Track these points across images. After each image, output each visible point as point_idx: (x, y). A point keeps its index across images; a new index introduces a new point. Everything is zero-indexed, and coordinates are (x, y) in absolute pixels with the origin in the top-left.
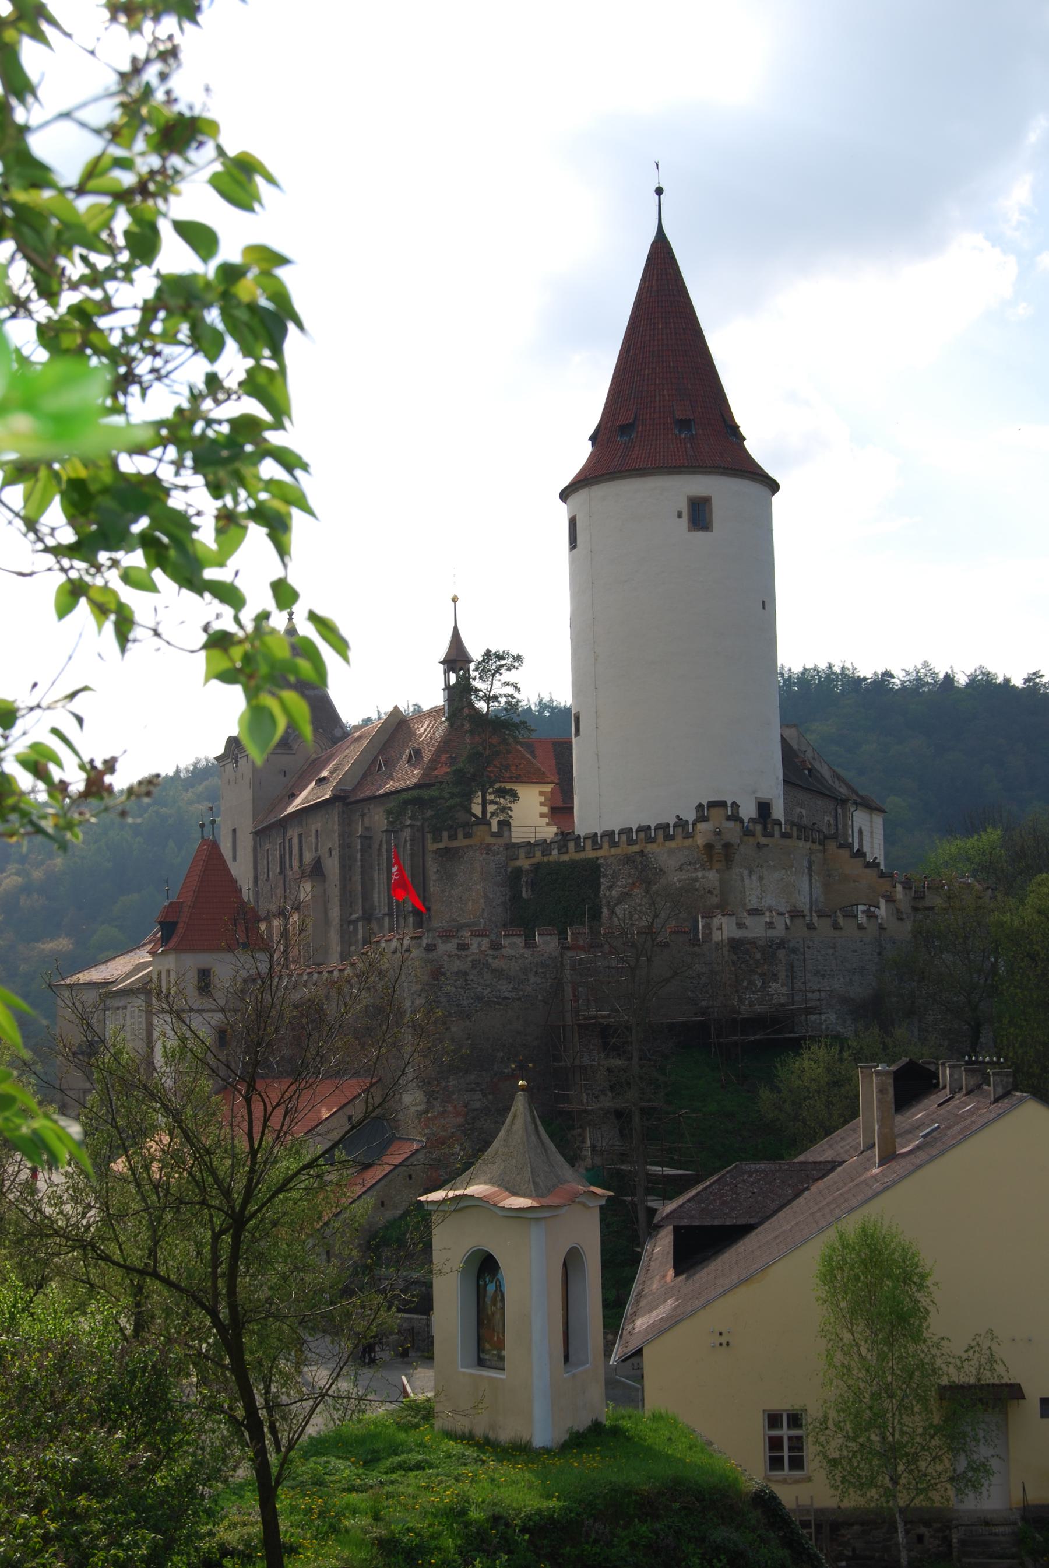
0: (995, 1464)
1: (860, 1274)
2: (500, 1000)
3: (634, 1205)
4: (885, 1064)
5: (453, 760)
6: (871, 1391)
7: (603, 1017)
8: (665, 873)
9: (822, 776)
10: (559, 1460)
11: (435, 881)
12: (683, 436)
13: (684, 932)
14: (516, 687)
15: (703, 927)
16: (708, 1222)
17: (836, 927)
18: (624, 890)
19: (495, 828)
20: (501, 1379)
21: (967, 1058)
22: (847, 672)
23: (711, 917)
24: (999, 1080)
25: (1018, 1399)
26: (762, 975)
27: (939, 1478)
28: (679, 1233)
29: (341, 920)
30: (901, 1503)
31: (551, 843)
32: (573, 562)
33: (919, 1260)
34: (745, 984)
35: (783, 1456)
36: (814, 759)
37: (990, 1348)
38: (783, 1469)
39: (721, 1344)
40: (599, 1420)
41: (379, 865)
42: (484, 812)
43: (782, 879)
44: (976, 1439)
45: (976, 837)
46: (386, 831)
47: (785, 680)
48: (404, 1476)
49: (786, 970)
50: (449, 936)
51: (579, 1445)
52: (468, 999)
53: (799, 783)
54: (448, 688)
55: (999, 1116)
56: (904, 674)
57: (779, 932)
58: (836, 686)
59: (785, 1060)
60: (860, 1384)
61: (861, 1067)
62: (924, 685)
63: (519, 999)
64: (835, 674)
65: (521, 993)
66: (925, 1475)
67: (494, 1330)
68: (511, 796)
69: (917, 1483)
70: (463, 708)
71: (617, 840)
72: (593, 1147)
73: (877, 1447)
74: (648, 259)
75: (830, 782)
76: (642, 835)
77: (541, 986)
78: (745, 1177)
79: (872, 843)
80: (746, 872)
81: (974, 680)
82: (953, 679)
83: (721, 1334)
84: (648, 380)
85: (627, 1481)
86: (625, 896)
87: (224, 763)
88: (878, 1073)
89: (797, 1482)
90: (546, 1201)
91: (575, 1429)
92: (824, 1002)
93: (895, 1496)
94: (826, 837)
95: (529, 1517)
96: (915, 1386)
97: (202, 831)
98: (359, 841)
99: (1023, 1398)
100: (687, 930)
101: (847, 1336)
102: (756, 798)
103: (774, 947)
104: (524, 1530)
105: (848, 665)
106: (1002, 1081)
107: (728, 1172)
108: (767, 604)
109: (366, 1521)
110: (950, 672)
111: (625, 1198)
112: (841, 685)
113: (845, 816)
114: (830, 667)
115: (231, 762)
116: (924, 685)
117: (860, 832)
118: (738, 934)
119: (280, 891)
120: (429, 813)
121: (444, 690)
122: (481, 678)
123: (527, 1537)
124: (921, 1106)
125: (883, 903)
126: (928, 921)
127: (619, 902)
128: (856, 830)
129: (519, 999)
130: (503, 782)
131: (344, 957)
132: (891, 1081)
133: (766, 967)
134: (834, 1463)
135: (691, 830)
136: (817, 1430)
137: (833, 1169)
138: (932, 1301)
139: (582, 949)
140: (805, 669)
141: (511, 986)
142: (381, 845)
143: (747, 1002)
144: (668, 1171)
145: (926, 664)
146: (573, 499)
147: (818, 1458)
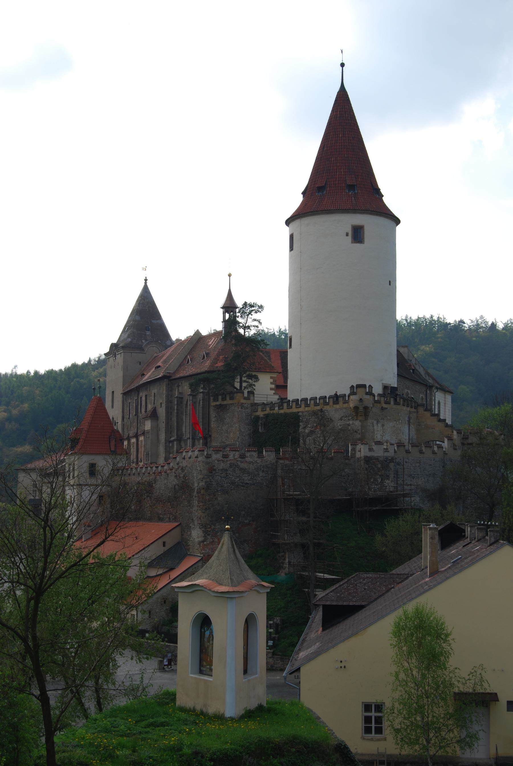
0: (481, 734)
1: (414, 632)
2: (244, 485)
4: (434, 524)
6: (417, 694)
7: (296, 495)
8: (333, 421)
9: (420, 373)
10: (237, 724)
11: (214, 422)
12: (350, 193)
13: (341, 452)
14: (259, 322)
15: (351, 450)
16: (340, 603)
17: (421, 452)
19: (246, 395)
20: (210, 681)
21: (479, 522)
22: (440, 320)
23: (356, 445)
24: (492, 534)
25: (496, 701)
26: (381, 476)
27: (452, 741)
28: (326, 608)
29: (166, 440)
30: (432, 753)
31: (275, 404)
32: (291, 257)
33: (444, 627)
34: (372, 480)
35: (371, 727)
36: (416, 364)
37: (480, 674)
38: (371, 733)
39: (341, 667)
40: (262, 704)
41: (186, 412)
42: (241, 386)
43: (394, 426)
44: (471, 721)
45: (498, 408)
46: (190, 395)
47: (408, 323)
48: (153, 729)
51: (250, 717)
53: (407, 376)
54: (224, 321)
55: (491, 553)
56: (470, 321)
58: (434, 327)
59: (390, 520)
60: (412, 690)
61: (424, 525)
62: (480, 328)
63: (254, 484)
64: (434, 320)
66: (444, 739)
68: (255, 378)
69: (440, 743)
70: (231, 332)
71: (309, 403)
72: (289, 562)
73: (420, 723)
74: (336, 100)
75: (424, 376)
76: (322, 401)
77: (266, 478)
79: (445, 409)
80: (375, 422)
81: (506, 326)
82: (496, 325)
83: (341, 662)
84: (333, 164)
85: (268, 736)
86: (312, 432)
87: (109, 357)
88: (430, 529)
89: (378, 740)
90: (236, 589)
91: (248, 709)
92: (413, 491)
93: (428, 749)
94: (418, 405)
95: (214, 754)
96: (440, 692)
98: (176, 400)
99: (499, 701)
100: (343, 451)
101: (406, 664)
103: (388, 461)
104: (211, 760)
105: (441, 316)
106: (494, 535)
107: (352, 578)
108: (391, 283)
109: (128, 752)
110: (494, 322)
111: (305, 590)
112: (437, 327)
113: (431, 394)
114: (432, 317)
115: (113, 356)
116: (480, 328)
117: (439, 403)
118: (369, 454)
119: (135, 424)
120: (212, 386)
121: (222, 322)
122: (241, 317)
123: (212, 763)
124: (455, 546)
125: (446, 440)
126: (469, 451)
127: (308, 435)
128: (437, 402)
129: (254, 484)
130: (251, 371)
131: (166, 459)
132: (437, 533)
134: (397, 731)
135: (347, 399)
136: (388, 713)
137: (407, 578)
138: (451, 648)
140: (419, 318)
141: (250, 477)
142: (187, 402)
143: (373, 490)
144: (327, 576)
145: (482, 317)
146: (294, 224)
147: (389, 728)
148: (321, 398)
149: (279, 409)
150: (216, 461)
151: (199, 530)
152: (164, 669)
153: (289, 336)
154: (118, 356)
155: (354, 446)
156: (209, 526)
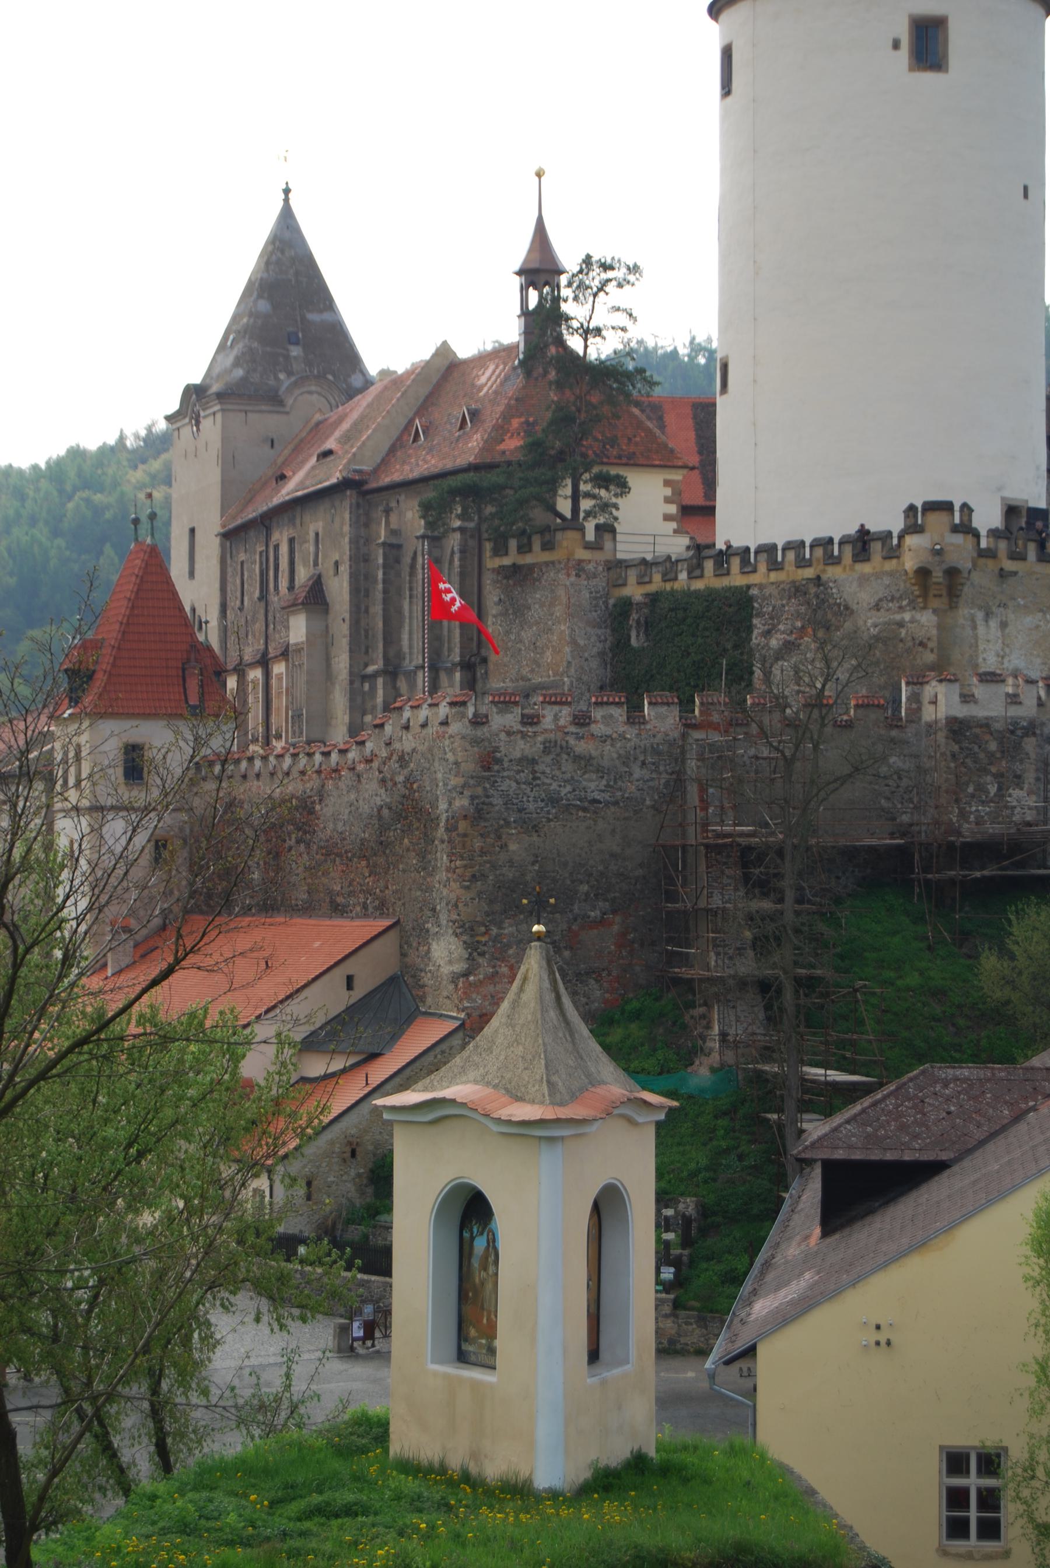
2: (586, 804)
3: (780, 1126)
5: (528, 427)
7: (742, 834)
8: (852, 612)
11: (495, 616)
13: (878, 706)
14: (631, 315)
15: (908, 699)
16: (876, 1155)
18: (788, 638)
19: (590, 535)
23: (922, 684)
26: (998, 776)
28: (834, 1171)
29: (351, 674)
31: (677, 561)
32: (725, 116)
39: (878, 1343)
40: (644, 1450)
41: (411, 589)
42: (575, 509)
43: (1038, 627)
48: (323, 1525)
49: (1037, 770)
50: (510, 702)
52: (535, 801)
54: (525, 313)
57: (1027, 710)
59: (1023, 910)
65: (619, 794)
67: (482, 1308)
71: (780, 559)
72: (723, 1035)
76: (819, 552)
77: (651, 784)
78: (938, 1088)
80: (980, 615)
83: (878, 1327)
85: (660, 1544)
86: (789, 647)
89: (988, 1557)
90: (564, 1113)
97: (136, 529)
98: (381, 551)
100: (882, 702)
102: (1003, 499)
103: (1019, 733)
118: (961, 711)
119: (259, 626)
120: (489, 509)
122: (576, 299)
127: (779, 656)
131: (354, 730)
133: (1004, 763)
139: (715, 727)
141: (604, 782)
143: (972, 818)
144: (836, 1076)
148: (816, 544)
149: (690, 578)
150: (503, 736)
151: (453, 939)
152: (352, 1349)
153: (719, 356)
154: (206, 424)
155: (916, 688)
156: (483, 929)
